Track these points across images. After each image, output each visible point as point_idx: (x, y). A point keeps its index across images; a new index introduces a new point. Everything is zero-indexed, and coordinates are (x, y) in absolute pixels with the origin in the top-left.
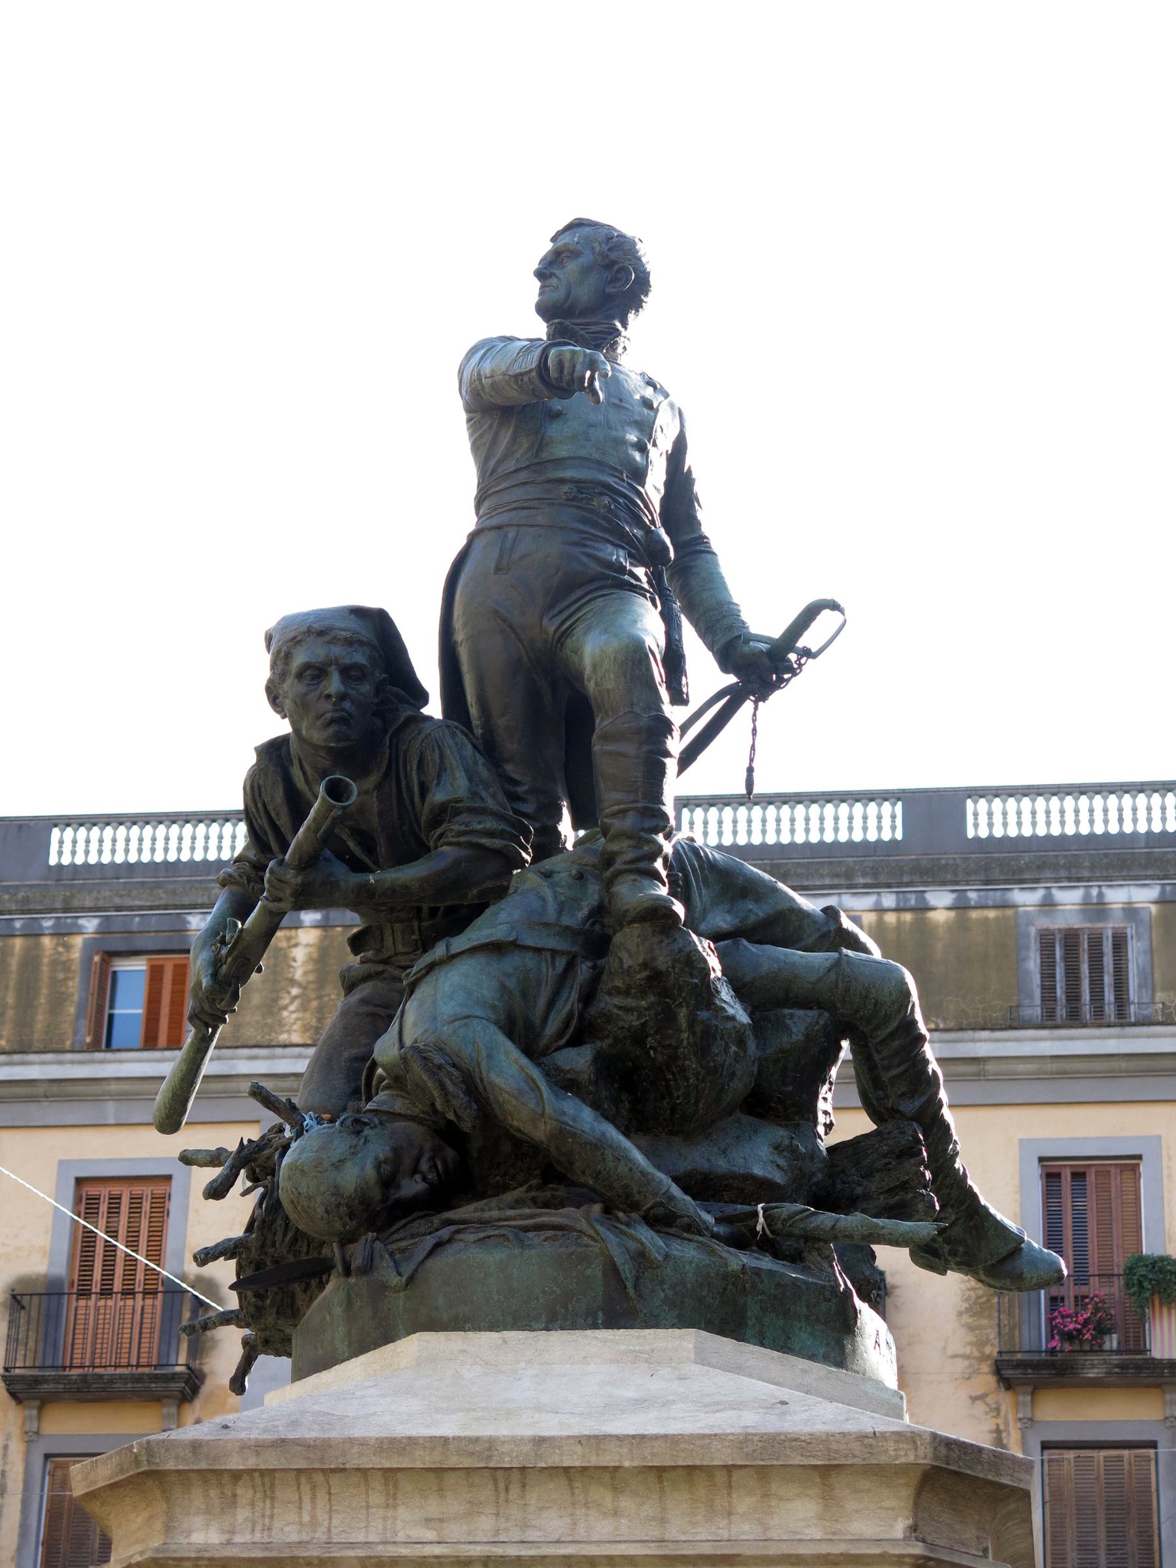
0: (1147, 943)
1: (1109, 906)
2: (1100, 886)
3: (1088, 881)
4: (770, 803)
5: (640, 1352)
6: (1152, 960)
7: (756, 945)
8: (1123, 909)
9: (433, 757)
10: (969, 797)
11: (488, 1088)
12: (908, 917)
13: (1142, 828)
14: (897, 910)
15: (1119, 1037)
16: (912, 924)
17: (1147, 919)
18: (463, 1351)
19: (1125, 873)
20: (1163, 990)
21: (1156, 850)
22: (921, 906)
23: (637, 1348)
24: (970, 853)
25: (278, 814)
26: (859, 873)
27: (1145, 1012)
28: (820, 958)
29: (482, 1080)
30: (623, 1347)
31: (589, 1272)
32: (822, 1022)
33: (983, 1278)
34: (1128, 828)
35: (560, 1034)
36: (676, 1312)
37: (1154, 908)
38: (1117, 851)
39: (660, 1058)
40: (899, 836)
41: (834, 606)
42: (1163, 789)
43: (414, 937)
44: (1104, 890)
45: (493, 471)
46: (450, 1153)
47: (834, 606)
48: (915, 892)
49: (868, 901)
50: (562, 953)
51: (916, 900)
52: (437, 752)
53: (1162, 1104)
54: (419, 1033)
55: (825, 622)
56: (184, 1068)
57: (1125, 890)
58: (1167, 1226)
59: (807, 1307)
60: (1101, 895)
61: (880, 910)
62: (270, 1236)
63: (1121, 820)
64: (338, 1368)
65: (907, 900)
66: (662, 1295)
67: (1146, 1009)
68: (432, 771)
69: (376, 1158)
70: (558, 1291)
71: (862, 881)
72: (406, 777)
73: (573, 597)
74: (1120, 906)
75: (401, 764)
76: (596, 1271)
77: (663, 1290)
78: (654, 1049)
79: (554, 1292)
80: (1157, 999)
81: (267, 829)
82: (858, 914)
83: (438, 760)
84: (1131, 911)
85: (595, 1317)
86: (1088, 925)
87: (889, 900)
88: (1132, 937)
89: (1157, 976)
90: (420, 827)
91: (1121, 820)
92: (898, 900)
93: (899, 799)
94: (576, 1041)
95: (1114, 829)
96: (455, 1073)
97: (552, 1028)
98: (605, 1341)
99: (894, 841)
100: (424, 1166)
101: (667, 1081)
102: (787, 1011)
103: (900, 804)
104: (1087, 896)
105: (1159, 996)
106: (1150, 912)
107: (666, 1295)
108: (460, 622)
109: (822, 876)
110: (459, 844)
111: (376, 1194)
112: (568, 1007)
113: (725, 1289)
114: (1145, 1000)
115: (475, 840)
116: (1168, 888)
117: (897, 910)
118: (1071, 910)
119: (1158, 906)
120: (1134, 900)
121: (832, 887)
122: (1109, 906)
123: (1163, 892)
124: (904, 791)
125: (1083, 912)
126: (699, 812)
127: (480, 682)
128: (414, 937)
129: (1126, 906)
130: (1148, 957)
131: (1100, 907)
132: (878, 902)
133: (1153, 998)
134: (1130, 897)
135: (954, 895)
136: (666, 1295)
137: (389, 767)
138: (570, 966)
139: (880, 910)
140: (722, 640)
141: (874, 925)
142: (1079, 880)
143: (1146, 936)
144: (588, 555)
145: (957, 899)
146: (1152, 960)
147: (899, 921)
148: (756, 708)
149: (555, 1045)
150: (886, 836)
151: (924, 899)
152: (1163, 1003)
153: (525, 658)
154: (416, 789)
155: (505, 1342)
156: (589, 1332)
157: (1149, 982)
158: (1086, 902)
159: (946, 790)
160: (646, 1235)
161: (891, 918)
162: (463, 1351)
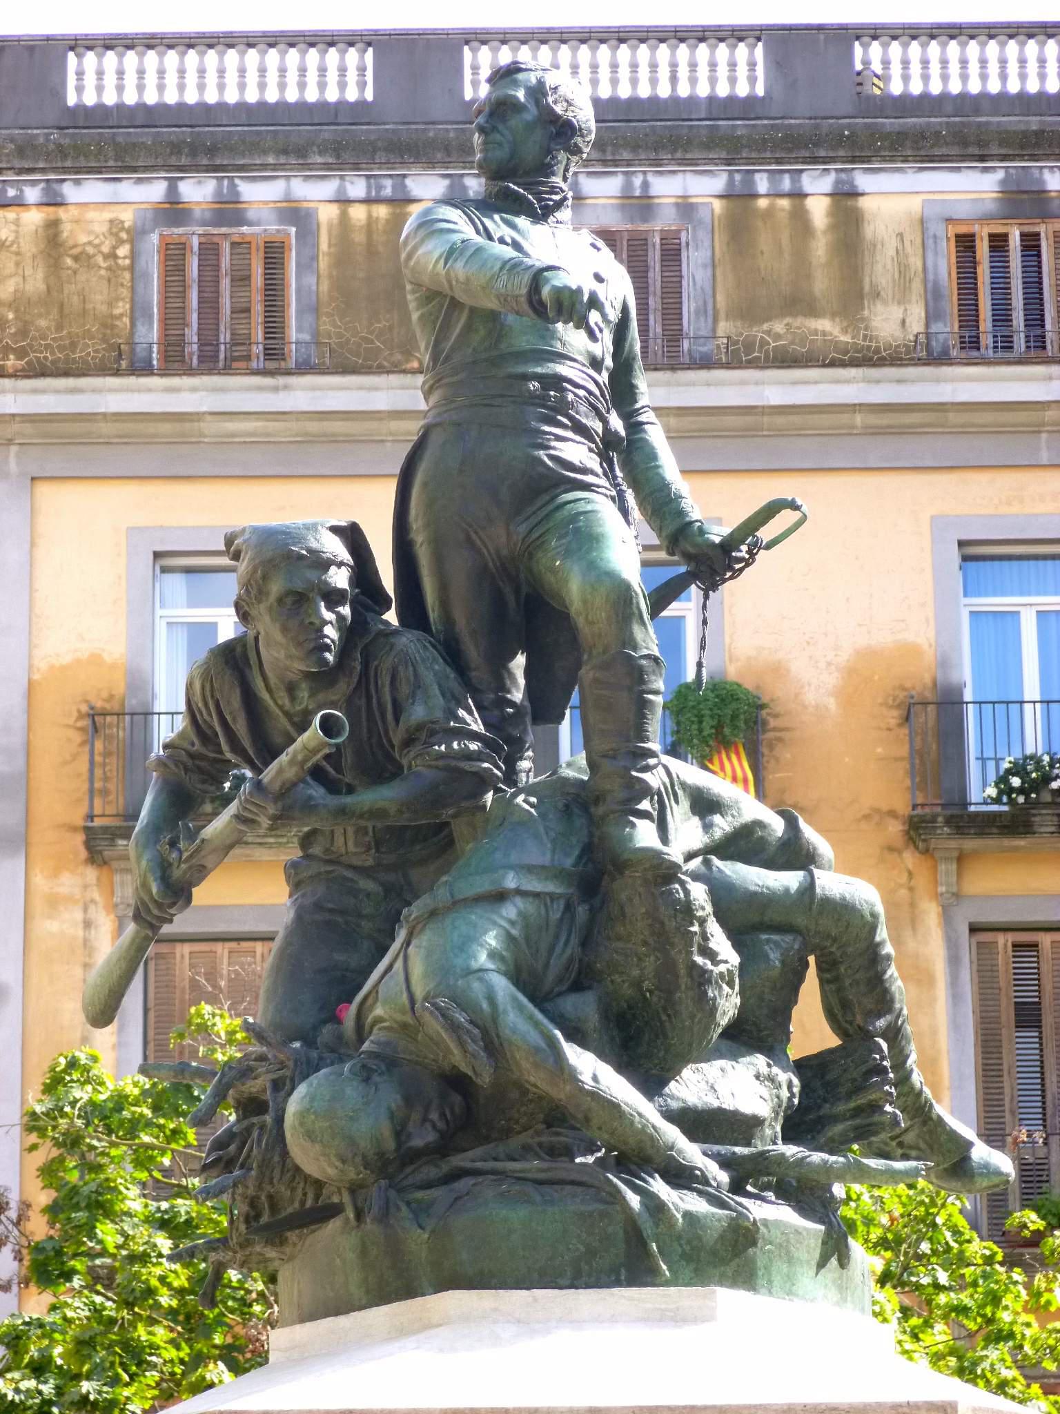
0: (709, 254)
1: (657, 201)
2: (644, 173)
3: (629, 165)
4: (191, 46)
5: (666, 1310)
6: (714, 276)
7: (728, 863)
8: (677, 204)
9: (405, 674)
10: (467, 42)
11: (505, 1045)
12: (382, 211)
13: (703, 91)
14: (367, 201)
15: (668, 384)
16: (387, 221)
17: (708, 219)
18: (496, 1310)
19: (679, 155)
20: (727, 319)
21: (721, 123)
22: (400, 196)
23: (663, 1306)
24: (465, 123)
25: (234, 719)
26: (315, 149)
27: (704, 349)
28: (791, 880)
29: (498, 1036)
30: (649, 1306)
31: (610, 1229)
32: (796, 947)
33: (934, 1180)
34: (684, 91)
35: (560, 980)
36: (692, 1266)
37: (718, 205)
38: (669, 123)
39: (655, 999)
40: (369, 95)
41: (794, 506)
42: (732, 36)
43: (367, 839)
44: (650, 178)
45: (447, 358)
46: (457, 1099)
47: (794, 506)
48: (390, 176)
49: (327, 188)
50: (560, 896)
51: (394, 187)
52: (411, 669)
53: (723, 475)
54: (432, 986)
55: (786, 518)
56: (124, 966)
57: (680, 177)
58: (727, 640)
59: (808, 1252)
60: (646, 185)
61: (343, 201)
62: (268, 1173)
63: (674, 79)
64: (355, 1315)
65: (380, 188)
66: (680, 1250)
67: (705, 345)
68: (404, 689)
69: (389, 1108)
70: (582, 1248)
71: (319, 160)
72: (377, 691)
73: (539, 503)
74: (673, 200)
75: (372, 680)
76: (617, 1230)
77: (681, 1246)
78: (651, 992)
79: (578, 1249)
80: (720, 333)
81: (218, 729)
82: (312, 205)
83: (412, 678)
84: (686, 207)
85: (618, 1274)
86: (629, 227)
87: (357, 188)
88: (688, 244)
89: (719, 298)
90: (393, 747)
91: (674, 79)
92: (369, 187)
93: (369, 44)
94: (577, 986)
95: (664, 91)
96: (476, 1031)
97: (551, 976)
98: (631, 1299)
99: (361, 104)
100: (434, 1116)
101: (661, 1022)
102: (764, 937)
103: (370, 50)
104: (628, 185)
105: (724, 327)
106: (713, 210)
107: (683, 1251)
108: (420, 523)
109: (265, 152)
110: (437, 767)
111: (390, 1145)
112: (569, 951)
113: (736, 1241)
114: (703, 333)
115: (453, 763)
116: (738, 177)
117: (367, 201)
118: (604, 206)
119: (724, 201)
120: (691, 192)
121: (275, 167)
122: (657, 201)
123: (731, 181)
124: (376, 33)
125: (622, 207)
126: (90, 57)
127: (443, 588)
128: (367, 839)
129: (680, 200)
130: (709, 272)
131: (645, 201)
132: (341, 190)
133: (714, 330)
134: (685, 189)
135: (446, 182)
136: (683, 1251)
137: (359, 682)
138: (569, 907)
139: (343, 201)
140: (671, 528)
141: (335, 222)
142: (616, 163)
143: (707, 243)
144: (551, 457)
145: (451, 187)
146: (714, 276)
147: (370, 216)
148: (706, 597)
149: (557, 990)
150: (352, 95)
151: (405, 186)
152: (728, 338)
153: (491, 564)
154: (389, 707)
155: (535, 1300)
156: (616, 1290)
157: (710, 307)
158: (626, 196)
159: (434, 32)
160: (658, 1186)
161: (358, 213)
162: (496, 1310)
